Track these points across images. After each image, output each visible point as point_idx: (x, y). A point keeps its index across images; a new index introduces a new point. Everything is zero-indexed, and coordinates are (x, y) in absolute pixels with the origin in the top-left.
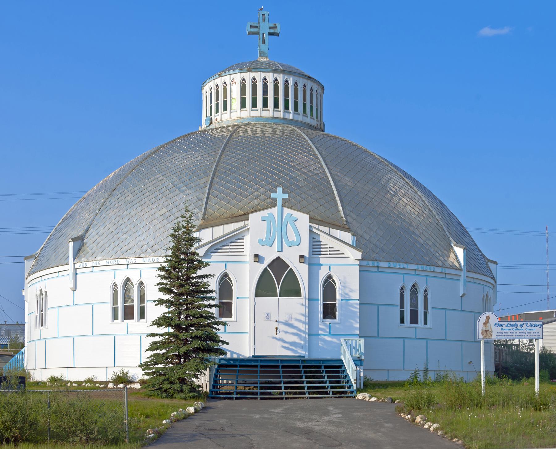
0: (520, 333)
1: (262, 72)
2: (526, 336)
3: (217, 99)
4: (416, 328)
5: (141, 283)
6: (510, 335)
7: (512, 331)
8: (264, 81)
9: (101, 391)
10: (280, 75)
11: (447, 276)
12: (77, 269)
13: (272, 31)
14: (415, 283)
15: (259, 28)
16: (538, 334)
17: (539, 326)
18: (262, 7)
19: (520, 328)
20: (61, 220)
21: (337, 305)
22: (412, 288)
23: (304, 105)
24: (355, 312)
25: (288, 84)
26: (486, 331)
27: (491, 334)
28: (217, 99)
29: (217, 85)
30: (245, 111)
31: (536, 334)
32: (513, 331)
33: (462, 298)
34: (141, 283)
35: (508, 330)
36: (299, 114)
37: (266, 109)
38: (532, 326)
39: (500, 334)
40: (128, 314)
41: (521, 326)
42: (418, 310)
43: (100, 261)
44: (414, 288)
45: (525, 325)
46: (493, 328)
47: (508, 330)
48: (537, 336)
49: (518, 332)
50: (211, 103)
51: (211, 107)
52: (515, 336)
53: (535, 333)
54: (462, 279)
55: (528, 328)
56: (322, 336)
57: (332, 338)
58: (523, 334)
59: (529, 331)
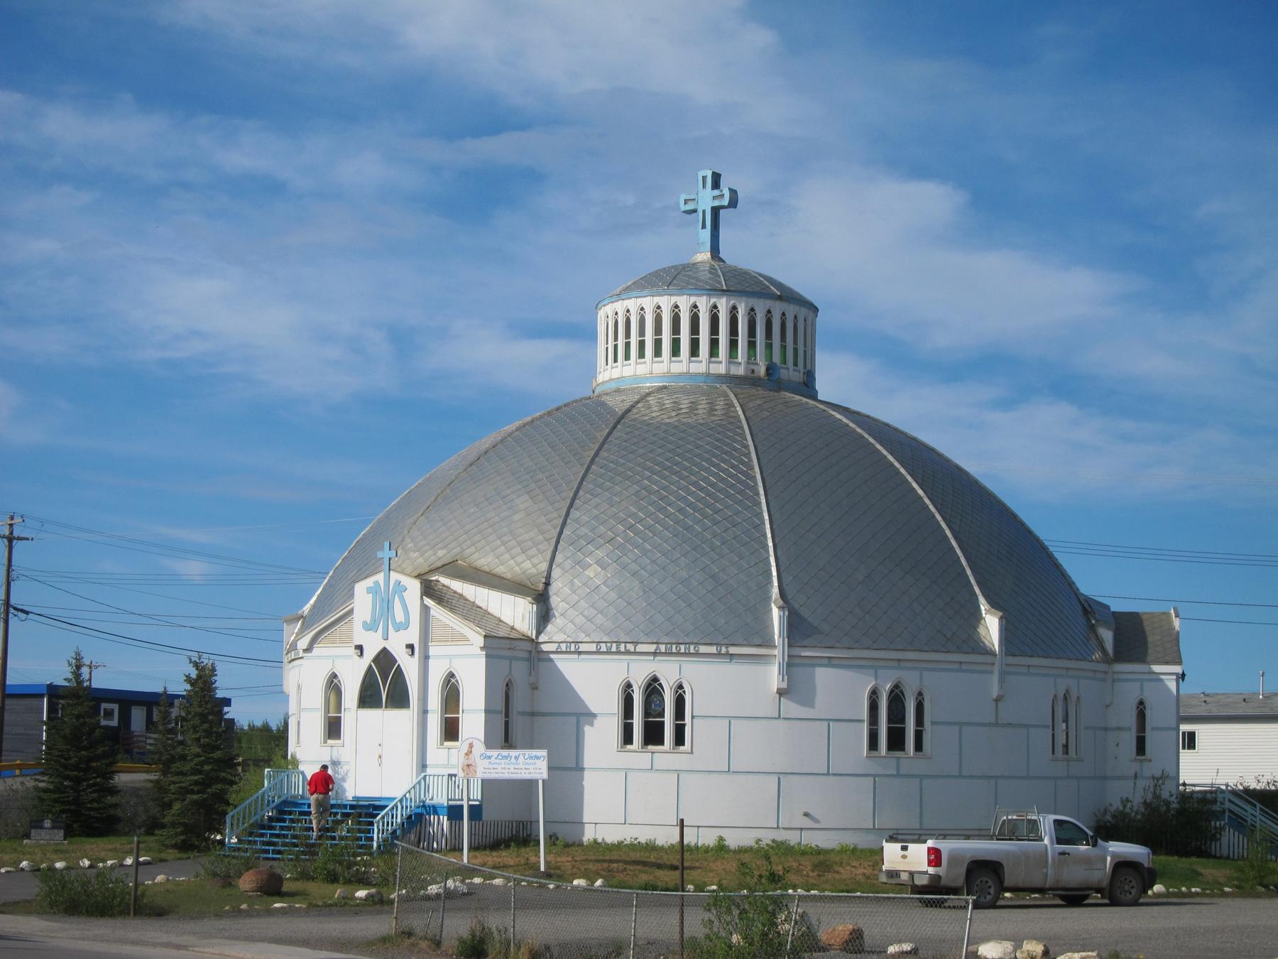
0: (515, 769)
1: (671, 295)
2: (523, 773)
3: (628, 335)
7: (503, 766)
8: (692, 310)
9: (652, 894)
10: (701, 298)
14: (899, 682)
16: (540, 771)
17: (542, 759)
19: (515, 761)
20: (341, 560)
25: (737, 312)
26: (468, 766)
27: (475, 771)
28: (628, 335)
30: (679, 362)
32: (506, 766)
33: (997, 705)
35: (499, 764)
39: (487, 771)
40: (653, 735)
41: (516, 758)
44: (653, 688)
45: (521, 757)
46: (478, 758)
47: (499, 764)
49: (512, 767)
50: (616, 339)
51: (616, 346)
53: (536, 768)
54: (996, 669)
55: (526, 761)
58: (519, 771)
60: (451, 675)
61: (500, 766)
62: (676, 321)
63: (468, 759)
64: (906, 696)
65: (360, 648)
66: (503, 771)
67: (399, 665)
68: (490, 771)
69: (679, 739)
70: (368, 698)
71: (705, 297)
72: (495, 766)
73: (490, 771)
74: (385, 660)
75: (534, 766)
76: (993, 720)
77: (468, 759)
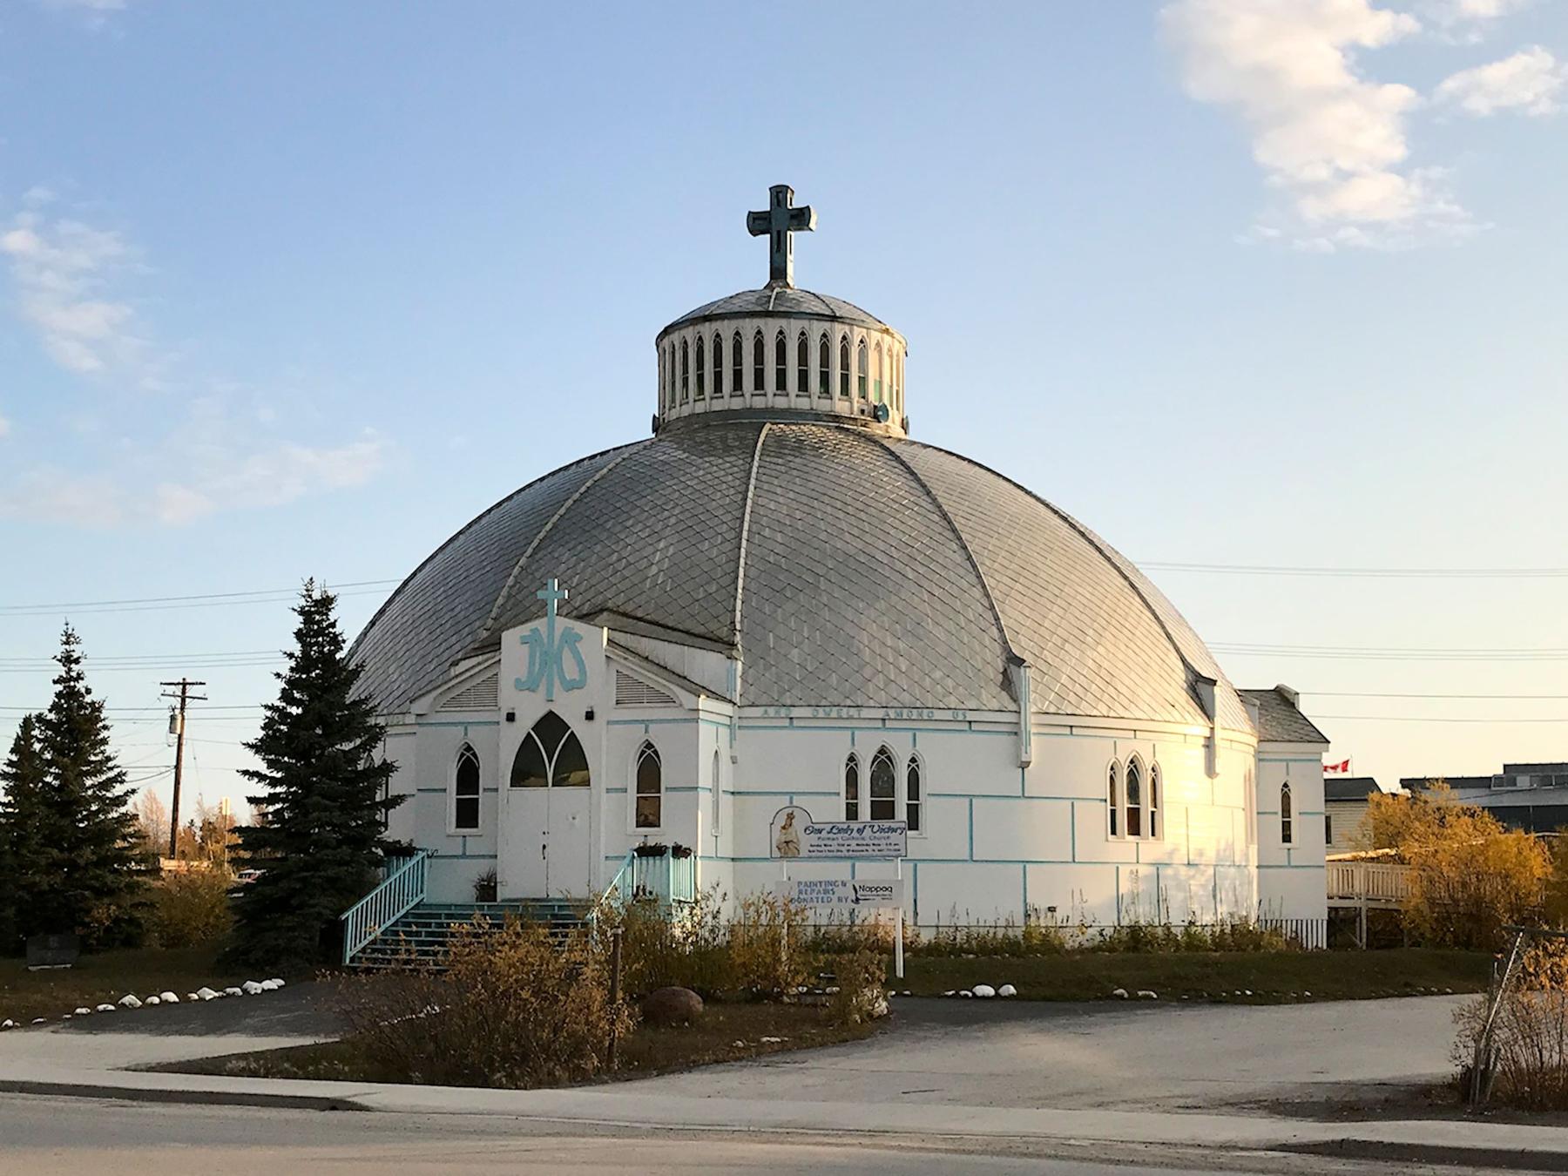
3: (686, 371)
4: (464, 837)
6: (838, 851)
7: (841, 842)
11: (796, 723)
16: (897, 847)
17: (899, 831)
22: (876, 758)
31: (892, 847)
38: (881, 830)
39: (815, 848)
42: (1138, 809)
44: (884, 761)
46: (801, 834)
48: (895, 850)
49: (854, 843)
52: (848, 851)
58: (864, 848)
59: (876, 842)
61: (835, 842)
64: (1140, 770)
65: (511, 717)
67: (572, 732)
68: (819, 849)
69: (913, 823)
70: (526, 771)
73: (819, 849)
74: (551, 725)
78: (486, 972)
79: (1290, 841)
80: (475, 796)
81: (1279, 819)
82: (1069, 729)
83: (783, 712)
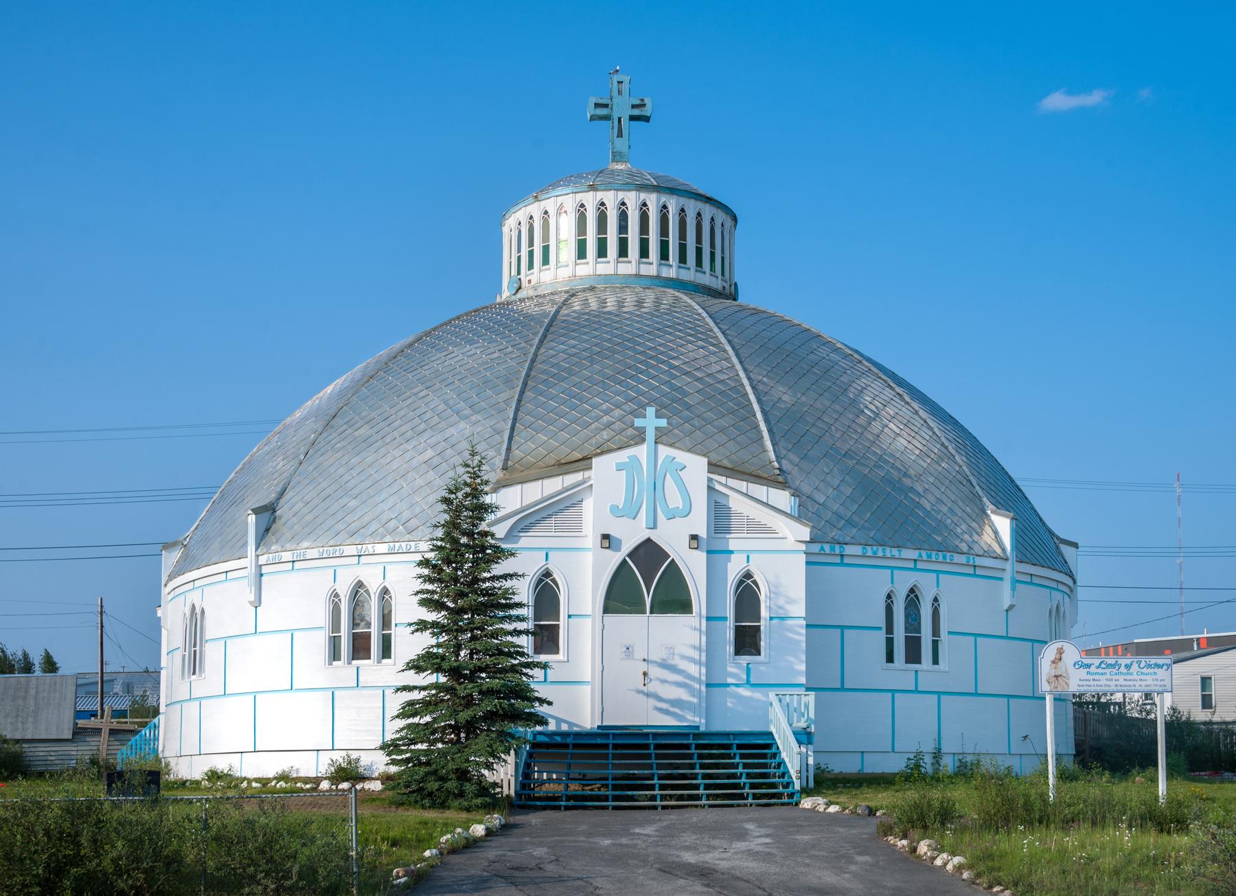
0: (1125, 680)
3: (531, 243)
5: (385, 591)
8: (620, 208)
11: (978, 572)
12: (263, 567)
13: (636, 112)
14: (914, 585)
15: (612, 108)
16: (1162, 683)
17: (1165, 667)
18: (618, 68)
21: (762, 628)
23: (699, 252)
24: (799, 642)
26: (1056, 677)
28: (531, 243)
29: (531, 217)
32: (1112, 677)
34: (385, 591)
36: (705, 273)
37: (625, 259)
39: (1084, 683)
40: (360, 648)
41: (1128, 667)
42: (920, 637)
43: (307, 550)
46: (1071, 669)
50: (519, 250)
51: (519, 258)
52: (1116, 686)
53: (1157, 680)
54: (1007, 576)
55: (1142, 670)
56: (733, 688)
57: (753, 692)
60: (748, 575)
61: (1104, 677)
62: (623, 217)
63: (1055, 668)
66: (1108, 683)
68: (1088, 683)
71: (634, 192)
72: (1096, 677)
73: (1088, 683)
75: (1155, 677)
76: (846, 631)
77: (1055, 668)
78: (51, 801)
79: (938, 664)
80: (888, 636)
81: (882, 635)
82: (1029, 577)
83: (837, 549)
